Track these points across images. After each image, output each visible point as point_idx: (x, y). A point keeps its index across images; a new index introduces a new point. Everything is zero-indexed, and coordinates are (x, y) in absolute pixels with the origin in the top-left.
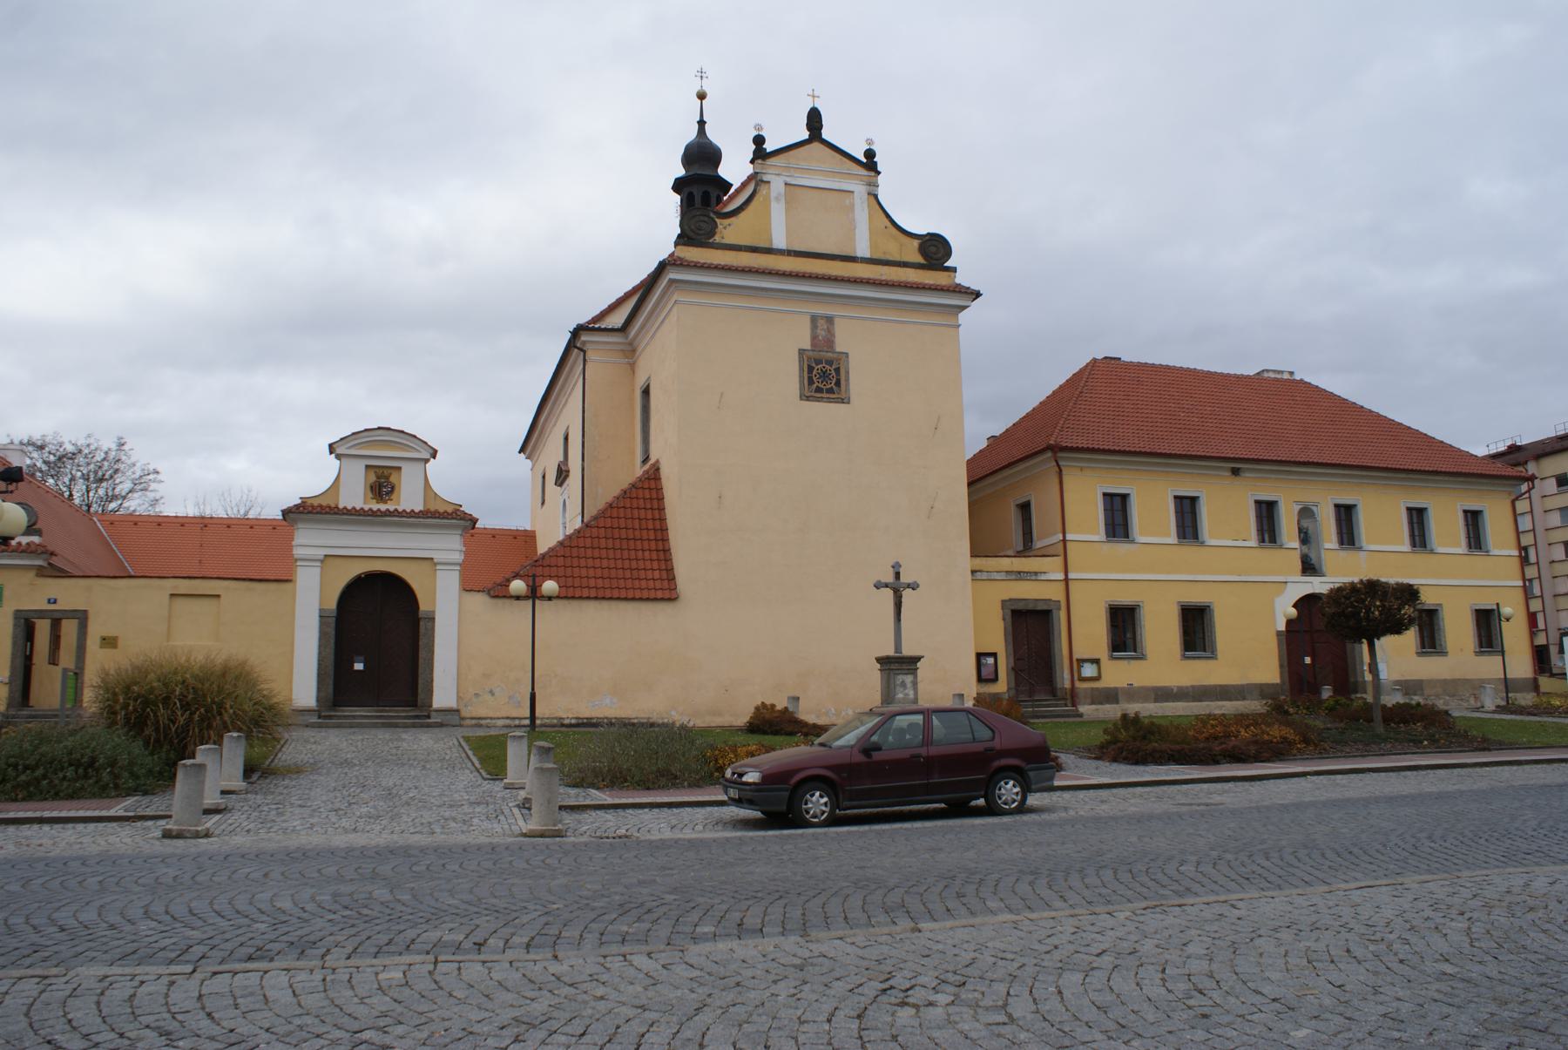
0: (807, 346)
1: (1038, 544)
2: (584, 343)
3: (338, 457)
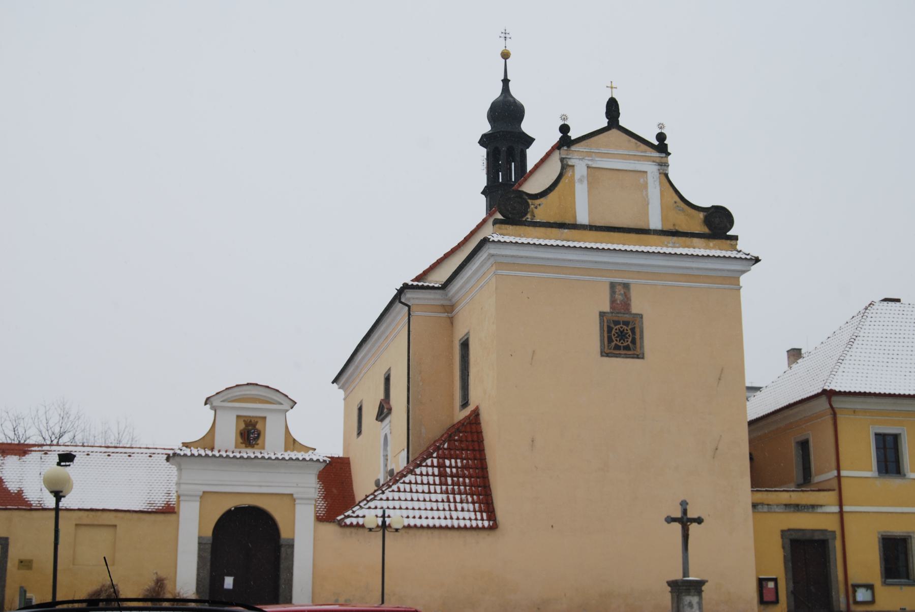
0: (606, 308)
1: (817, 479)
2: (409, 299)
3: (215, 409)
